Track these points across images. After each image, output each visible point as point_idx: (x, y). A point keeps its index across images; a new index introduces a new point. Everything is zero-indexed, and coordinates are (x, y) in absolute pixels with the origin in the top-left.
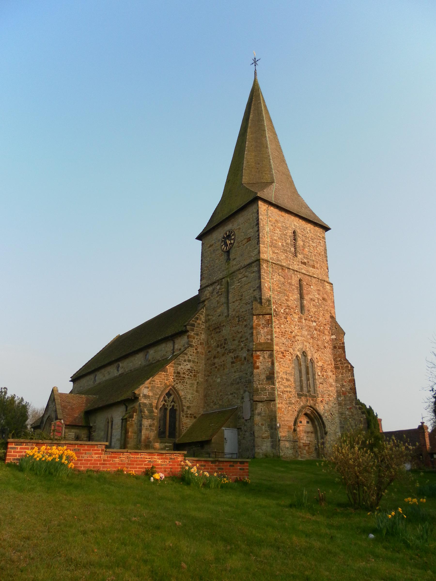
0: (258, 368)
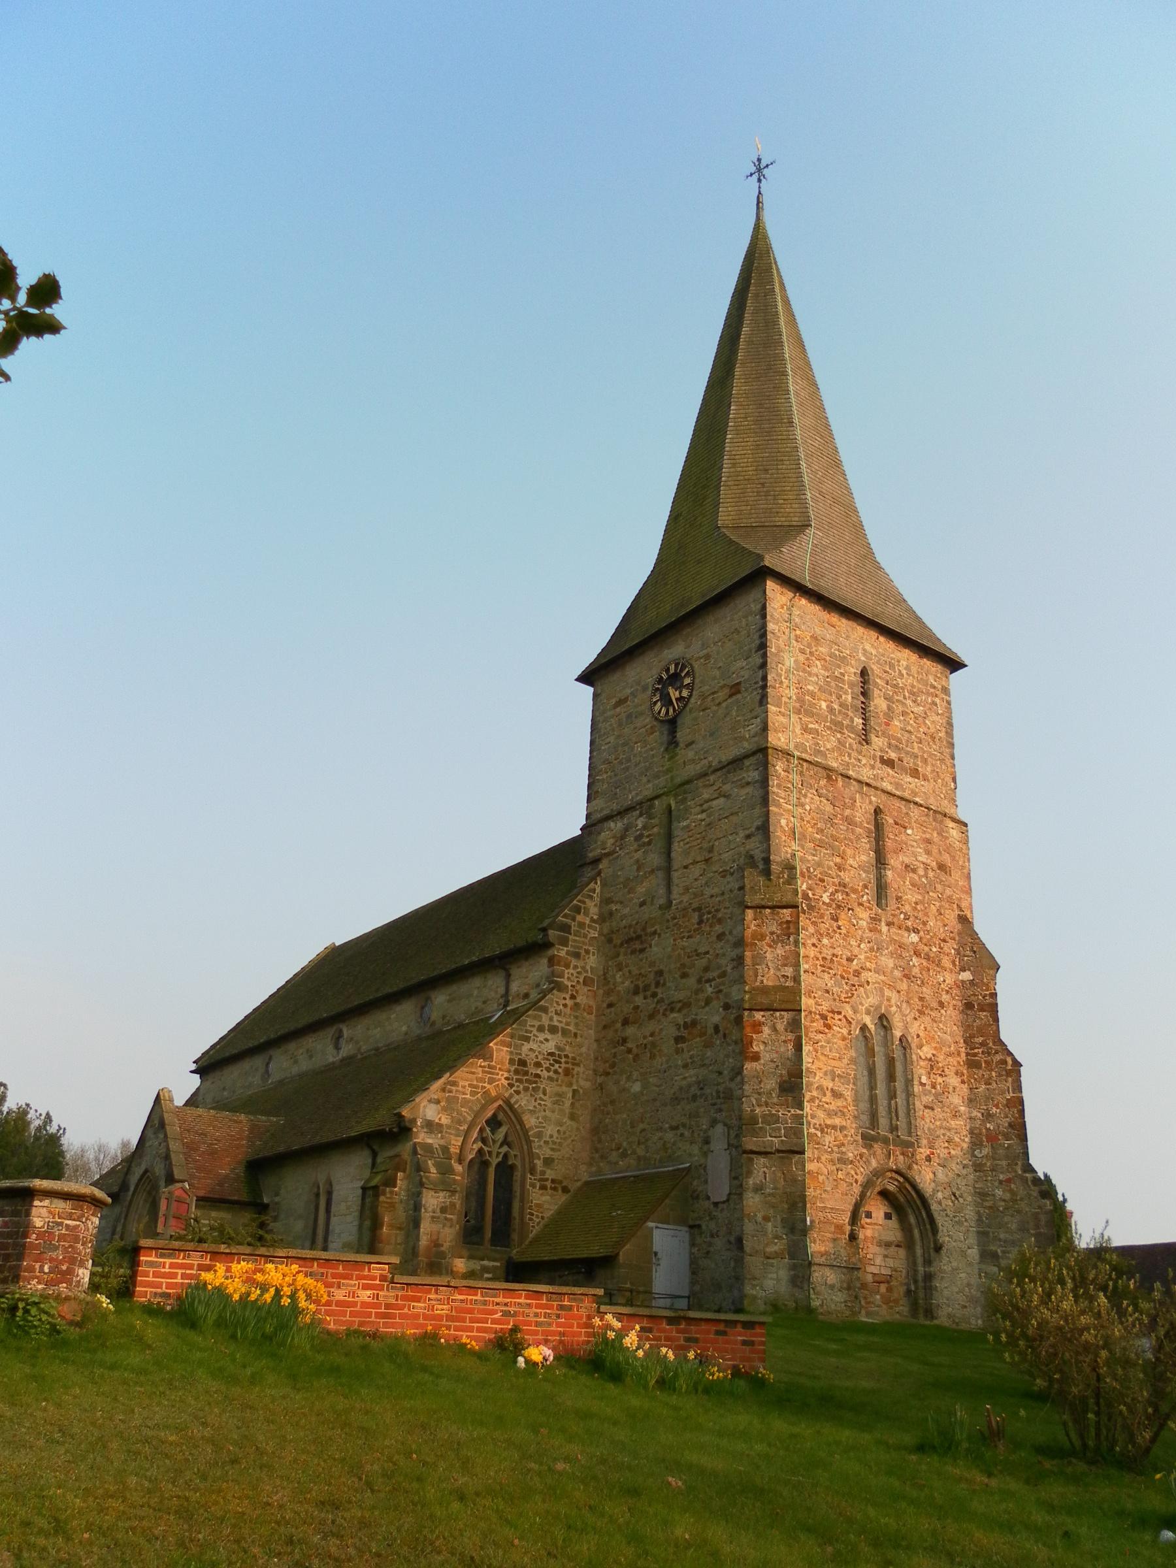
0: (756, 1057)
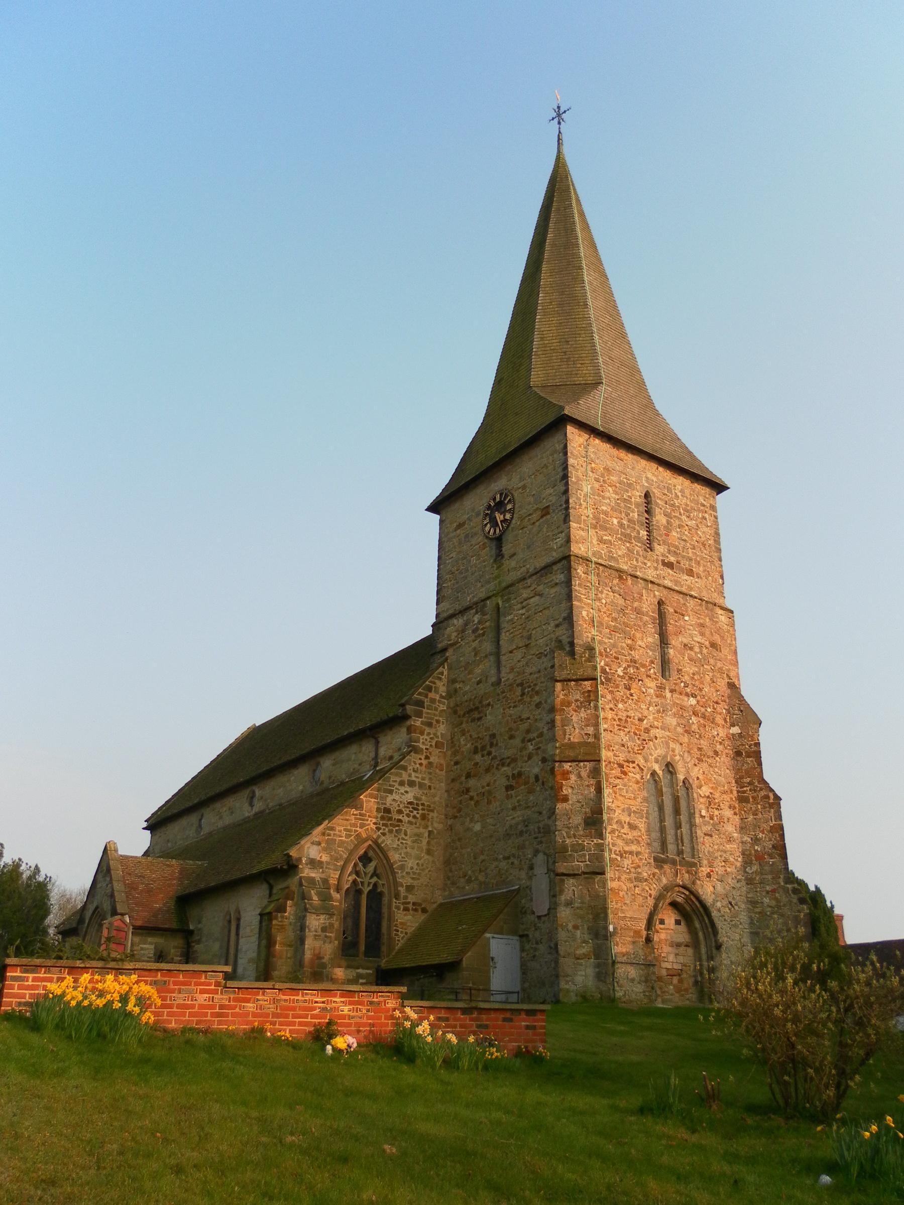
0: (565, 799)
